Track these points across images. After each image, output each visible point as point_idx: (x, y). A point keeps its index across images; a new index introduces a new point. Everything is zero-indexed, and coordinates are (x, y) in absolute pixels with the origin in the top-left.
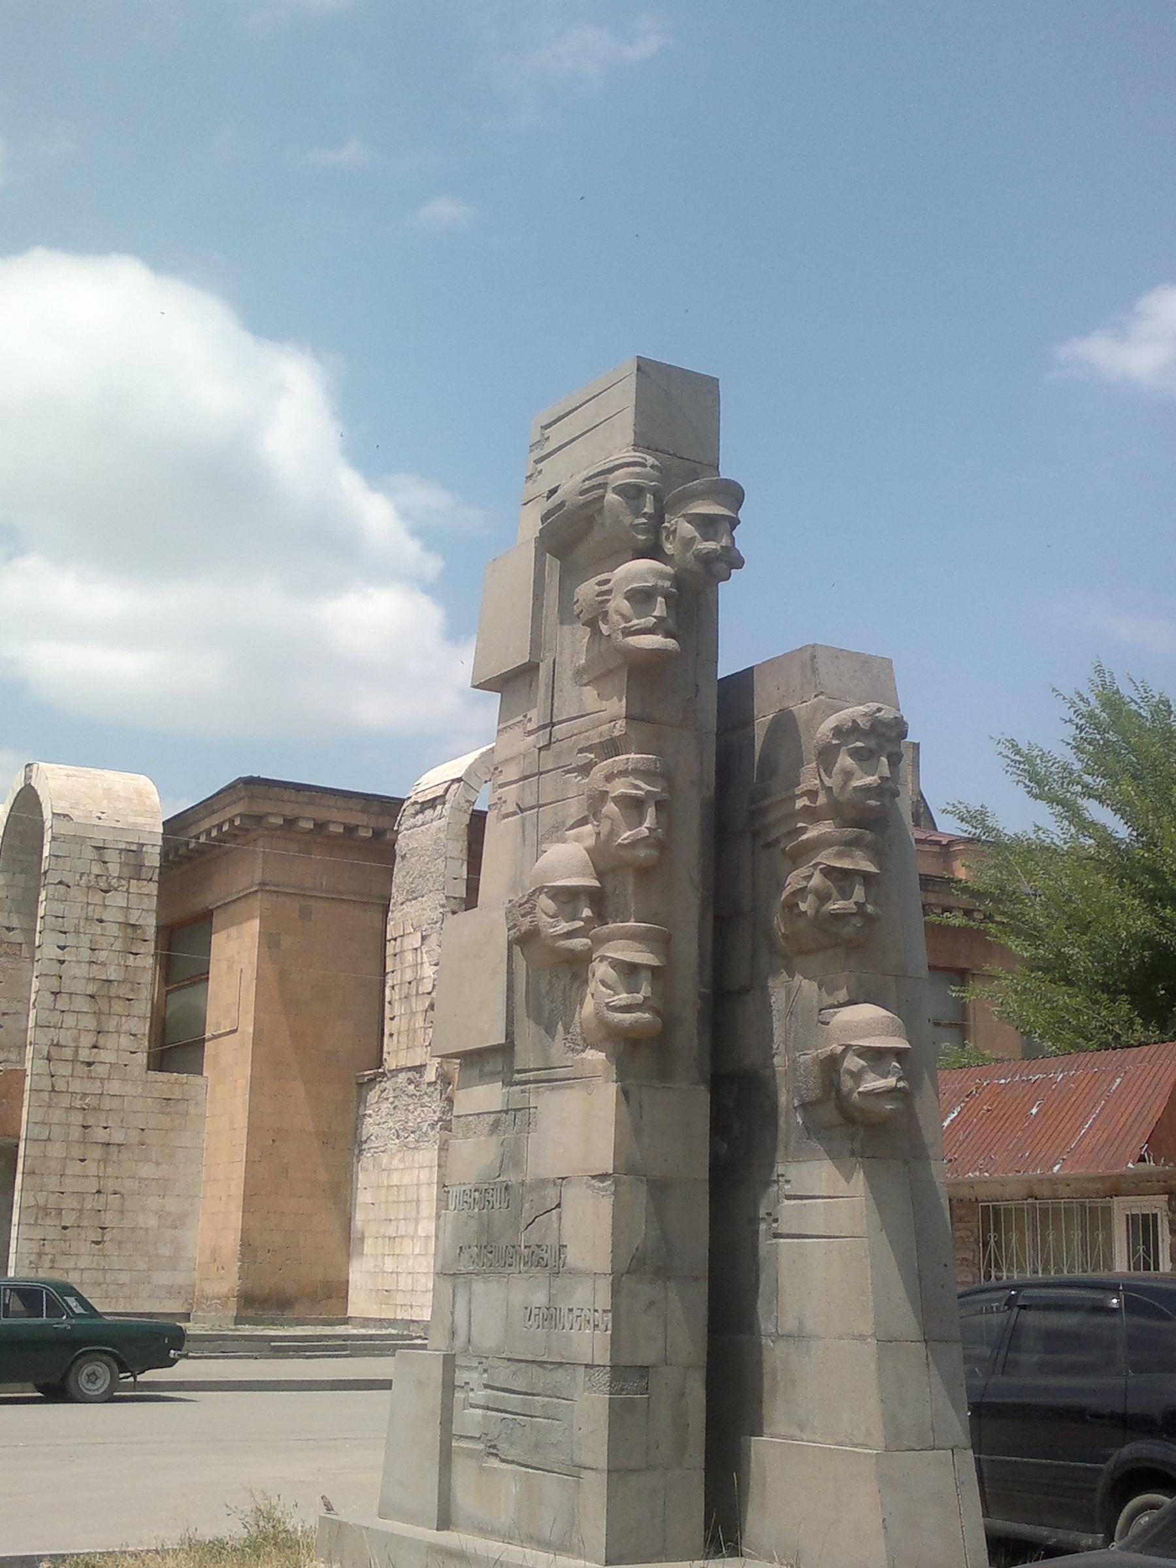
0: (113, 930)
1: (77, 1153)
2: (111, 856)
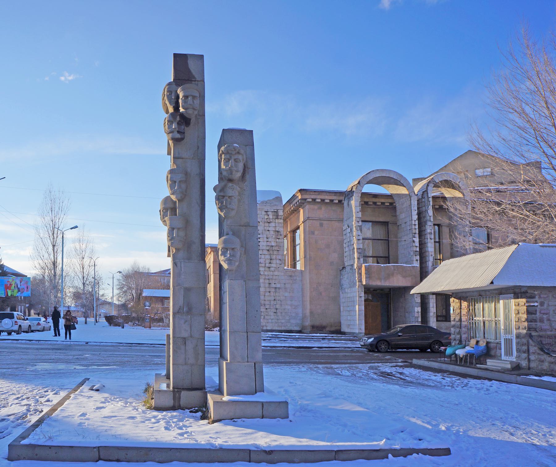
0: (272, 233)
1: (268, 290)
2: (270, 213)
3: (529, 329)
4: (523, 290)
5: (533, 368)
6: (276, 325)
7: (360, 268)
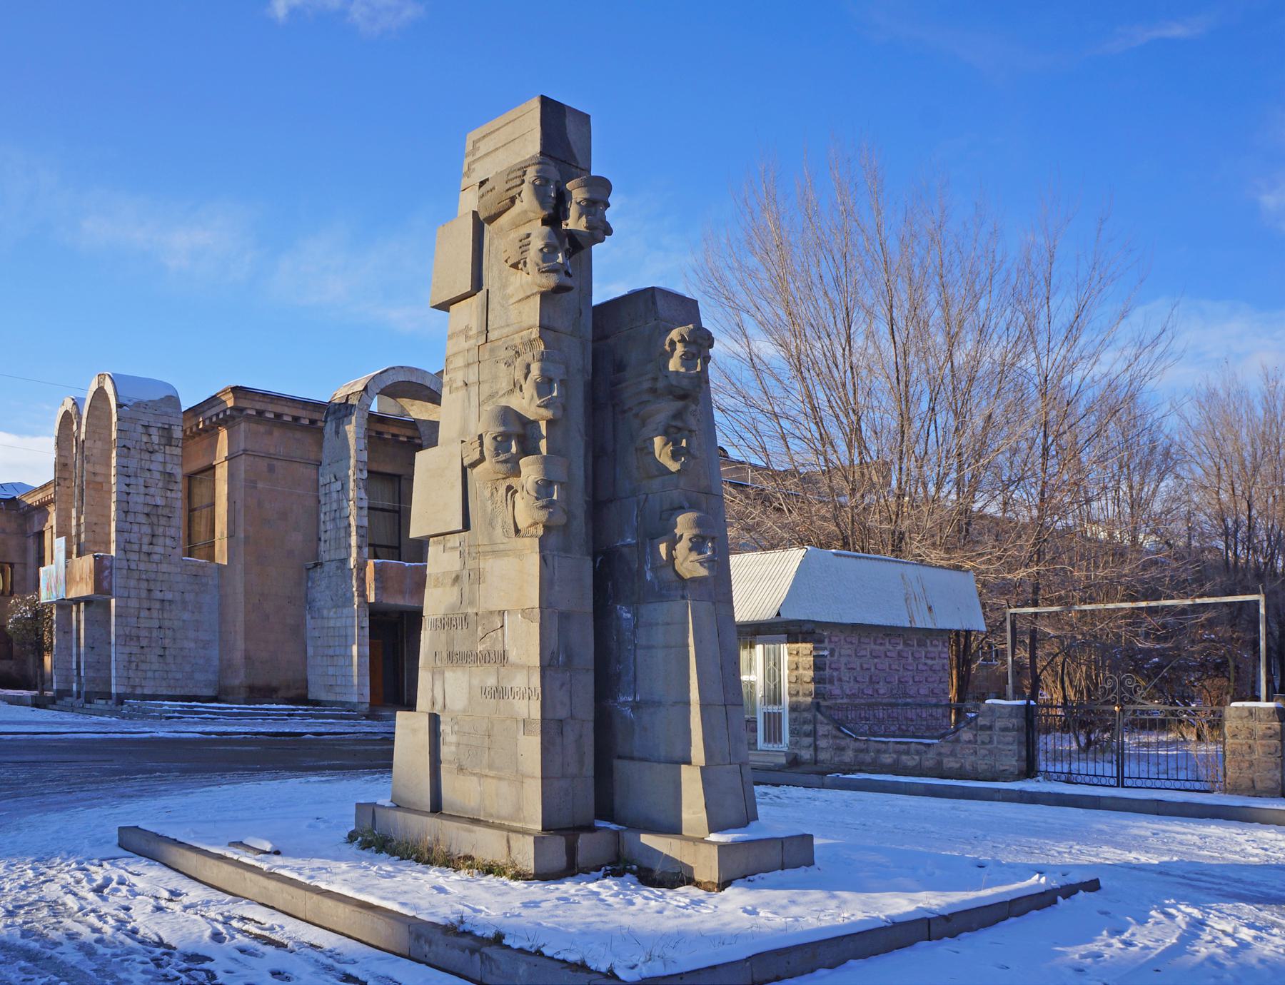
0: (157, 475)
1: (146, 605)
2: (153, 431)
3: (817, 694)
4: (804, 629)
5: (823, 762)
6: (164, 683)
7: (361, 568)
